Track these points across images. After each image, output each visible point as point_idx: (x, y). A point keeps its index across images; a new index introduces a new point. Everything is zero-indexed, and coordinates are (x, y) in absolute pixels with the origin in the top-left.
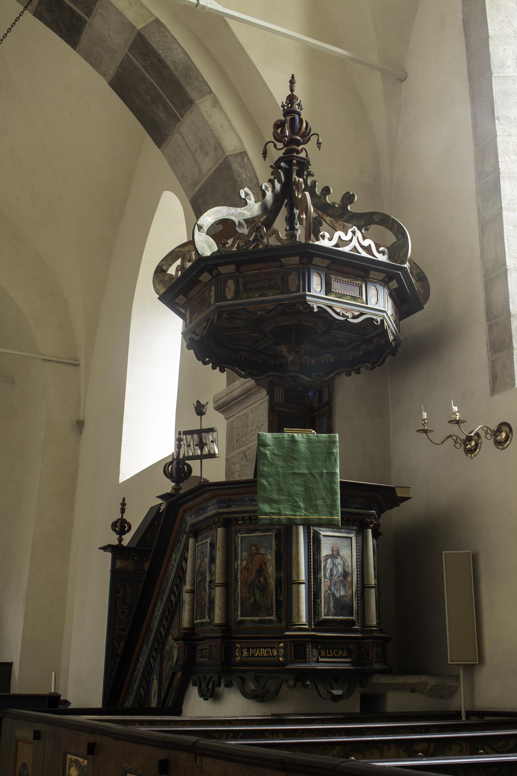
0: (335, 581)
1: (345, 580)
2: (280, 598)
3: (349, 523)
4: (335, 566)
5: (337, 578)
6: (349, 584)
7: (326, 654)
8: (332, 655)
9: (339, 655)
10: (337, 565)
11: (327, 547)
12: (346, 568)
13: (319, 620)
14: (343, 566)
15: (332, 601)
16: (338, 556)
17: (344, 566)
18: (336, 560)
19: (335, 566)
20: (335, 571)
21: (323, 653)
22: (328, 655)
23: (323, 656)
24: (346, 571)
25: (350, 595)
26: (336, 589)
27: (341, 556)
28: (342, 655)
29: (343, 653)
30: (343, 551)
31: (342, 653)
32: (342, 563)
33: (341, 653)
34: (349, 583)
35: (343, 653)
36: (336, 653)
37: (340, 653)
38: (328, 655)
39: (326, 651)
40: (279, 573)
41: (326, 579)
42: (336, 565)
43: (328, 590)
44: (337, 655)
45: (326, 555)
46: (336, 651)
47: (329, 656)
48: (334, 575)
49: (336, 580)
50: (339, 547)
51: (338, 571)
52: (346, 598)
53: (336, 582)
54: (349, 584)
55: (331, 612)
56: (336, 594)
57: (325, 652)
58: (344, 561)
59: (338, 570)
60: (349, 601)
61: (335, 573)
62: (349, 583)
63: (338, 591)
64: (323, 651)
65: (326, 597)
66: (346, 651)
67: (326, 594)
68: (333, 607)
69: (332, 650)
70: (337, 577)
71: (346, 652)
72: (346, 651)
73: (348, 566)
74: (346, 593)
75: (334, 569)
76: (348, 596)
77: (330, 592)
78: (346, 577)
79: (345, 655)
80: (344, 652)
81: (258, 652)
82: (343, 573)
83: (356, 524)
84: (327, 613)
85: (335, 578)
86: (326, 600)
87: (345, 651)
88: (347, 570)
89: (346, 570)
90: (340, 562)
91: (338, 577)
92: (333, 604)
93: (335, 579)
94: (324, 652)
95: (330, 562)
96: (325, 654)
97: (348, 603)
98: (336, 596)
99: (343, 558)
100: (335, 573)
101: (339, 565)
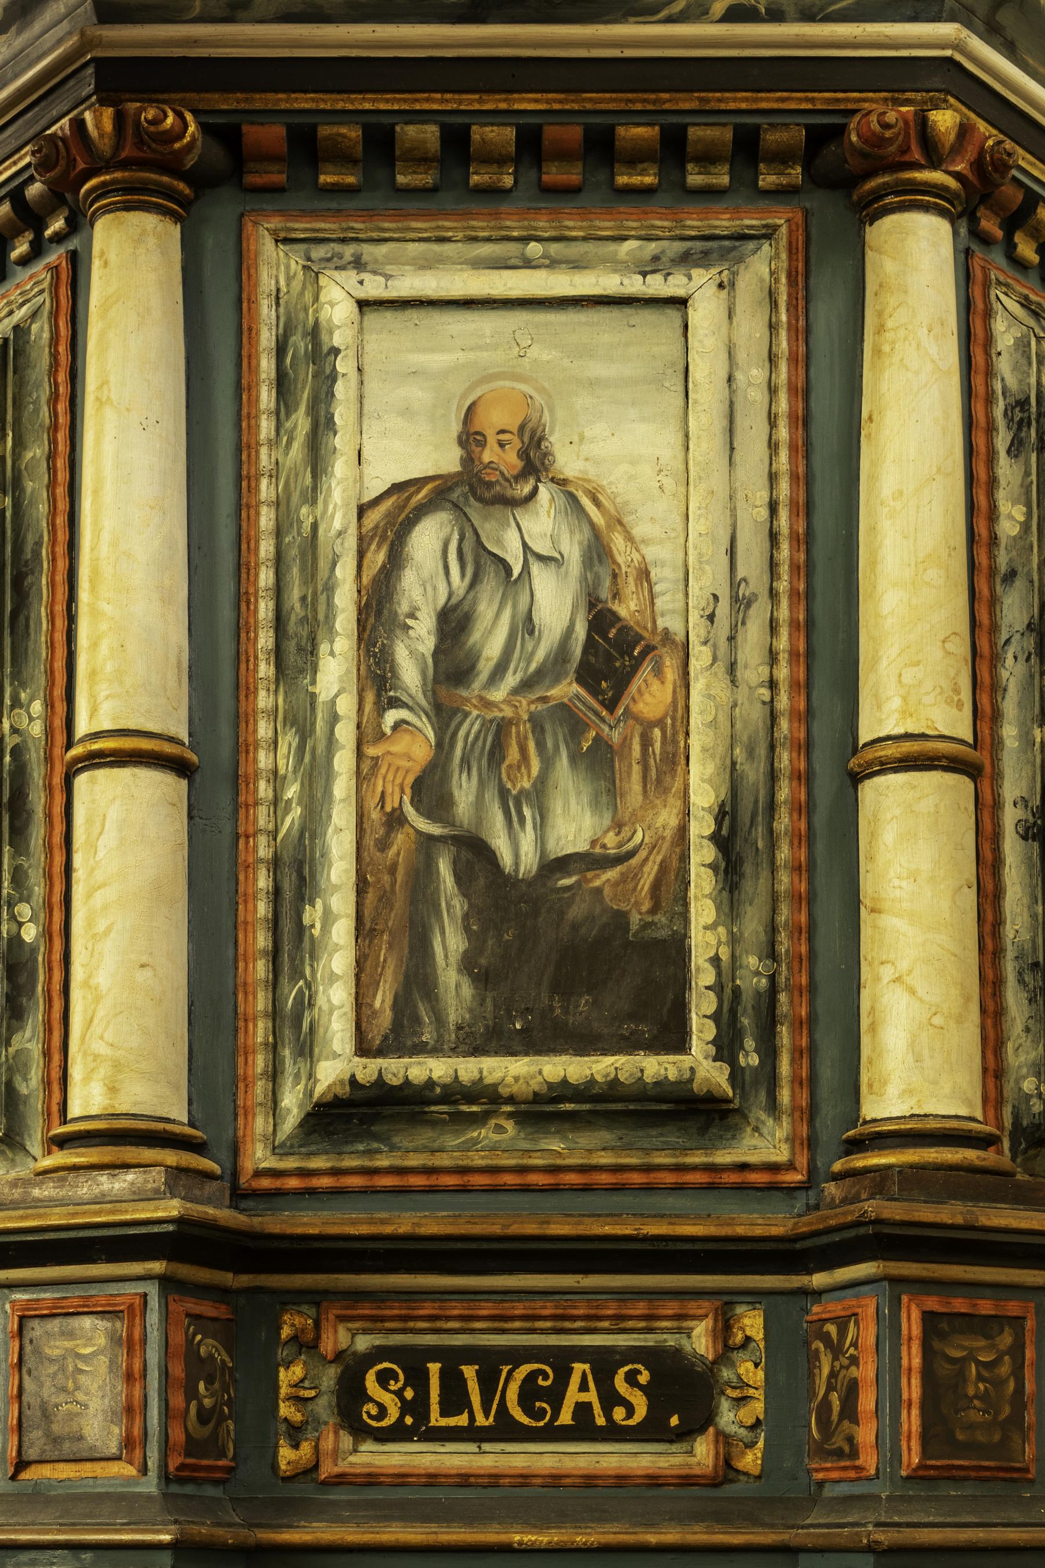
0: (486, 724)
1: (611, 706)
2: (20, 925)
3: (695, 179)
4: (490, 586)
5: (515, 691)
6: (646, 742)
7: (418, 1407)
8: (481, 1420)
9: (566, 1417)
10: (516, 572)
11: (406, 412)
12: (616, 595)
13: (319, 1089)
14: (583, 579)
15: (459, 913)
16: (527, 489)
17: (597, 578)
18: (505, 525)
19: (490, 586)
20: (489, 632)
21: (387, 1399)
22: (444, 1413)
23: (385, 1423)
24: (616, 617)
25: (666, 845)
26: (503, 794)
27: (562, 482)
28: (601, 1421)
29: (610, 1399)
30: (588, 433)
31: (592, 1396)
32: (572, 549)
33: (584, 1397)
34: (657, 733)
35: (610, 1399)
36: (529, 1394)
37: (573, 1395)
38: (444, 1413)
39: (418, 1379)
40: (13, 707)
41: (395, 703)
42: (508, 569)
43: (409, 810)
44: (528, 1411)
45: (397, 488)
46: (531, 1377)
47: (444, 1422)
48: (485, 668)
49: (508, 712)
50: (539, 399)
51: (527, 625)
52: (612, 874)
53: (501, 729)
54: (646, 742)
55: (439, 1020)
56: (501, 844)
57: (409, 1394)
58: (592, 525)
59: (529, 618)
60: (646, 906)
61: (493, 649)
62: (657, 733)
63: (527, 812)
64: (384, 1379)
65: (392, 870)
66: (644, 1378)
67: (383, 845)
68: (468, 964)
69: (480, 1375)
70: (511, 680)
71: (371, 1400)
72: (644, 1378)
73: (644, 574)
74: (618, 826)
75: (485, 609)
76: (634, 861)
77: (435, 829)
78: (622, 681)
79: (630, 1411)
80: (620, 1384)
81: (584, 1387)
82: (590, 644)
83: (768, 180)
84: (397, 1026)
85: (498, 695)
86: (385, 899)
87: (631, 1379)
88: (627, 609)
89: (622, 611)
90: (554, 541)
91: (526, 685)
92: (467, 929)
93: (488, 704)
94: (399, 1393)
95: (438, 547)
96: (406, 1407)
97: (635, 919)
98: (506, 859)
99: (586, 502)
100: (493, 649)
101: (535, 568)
